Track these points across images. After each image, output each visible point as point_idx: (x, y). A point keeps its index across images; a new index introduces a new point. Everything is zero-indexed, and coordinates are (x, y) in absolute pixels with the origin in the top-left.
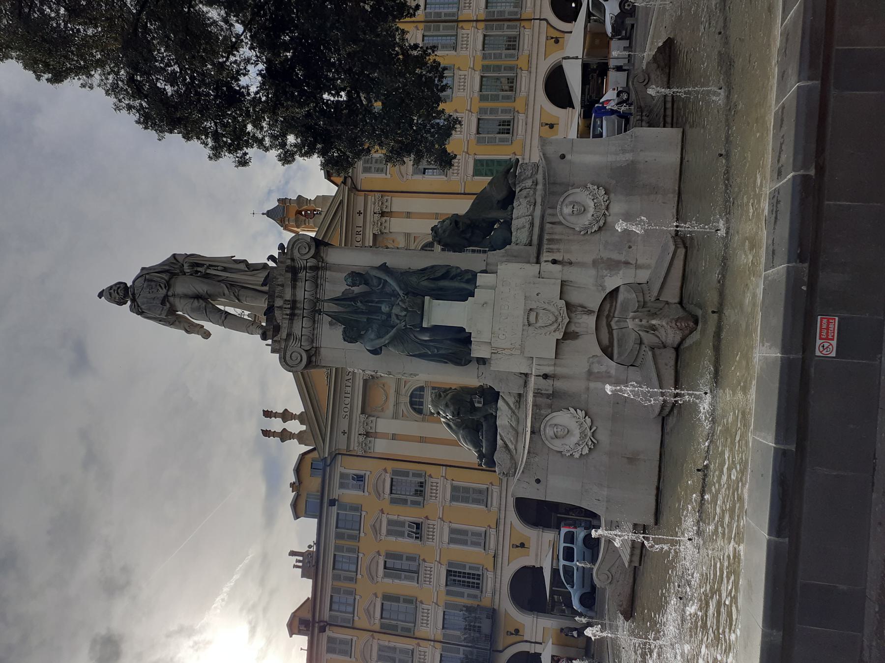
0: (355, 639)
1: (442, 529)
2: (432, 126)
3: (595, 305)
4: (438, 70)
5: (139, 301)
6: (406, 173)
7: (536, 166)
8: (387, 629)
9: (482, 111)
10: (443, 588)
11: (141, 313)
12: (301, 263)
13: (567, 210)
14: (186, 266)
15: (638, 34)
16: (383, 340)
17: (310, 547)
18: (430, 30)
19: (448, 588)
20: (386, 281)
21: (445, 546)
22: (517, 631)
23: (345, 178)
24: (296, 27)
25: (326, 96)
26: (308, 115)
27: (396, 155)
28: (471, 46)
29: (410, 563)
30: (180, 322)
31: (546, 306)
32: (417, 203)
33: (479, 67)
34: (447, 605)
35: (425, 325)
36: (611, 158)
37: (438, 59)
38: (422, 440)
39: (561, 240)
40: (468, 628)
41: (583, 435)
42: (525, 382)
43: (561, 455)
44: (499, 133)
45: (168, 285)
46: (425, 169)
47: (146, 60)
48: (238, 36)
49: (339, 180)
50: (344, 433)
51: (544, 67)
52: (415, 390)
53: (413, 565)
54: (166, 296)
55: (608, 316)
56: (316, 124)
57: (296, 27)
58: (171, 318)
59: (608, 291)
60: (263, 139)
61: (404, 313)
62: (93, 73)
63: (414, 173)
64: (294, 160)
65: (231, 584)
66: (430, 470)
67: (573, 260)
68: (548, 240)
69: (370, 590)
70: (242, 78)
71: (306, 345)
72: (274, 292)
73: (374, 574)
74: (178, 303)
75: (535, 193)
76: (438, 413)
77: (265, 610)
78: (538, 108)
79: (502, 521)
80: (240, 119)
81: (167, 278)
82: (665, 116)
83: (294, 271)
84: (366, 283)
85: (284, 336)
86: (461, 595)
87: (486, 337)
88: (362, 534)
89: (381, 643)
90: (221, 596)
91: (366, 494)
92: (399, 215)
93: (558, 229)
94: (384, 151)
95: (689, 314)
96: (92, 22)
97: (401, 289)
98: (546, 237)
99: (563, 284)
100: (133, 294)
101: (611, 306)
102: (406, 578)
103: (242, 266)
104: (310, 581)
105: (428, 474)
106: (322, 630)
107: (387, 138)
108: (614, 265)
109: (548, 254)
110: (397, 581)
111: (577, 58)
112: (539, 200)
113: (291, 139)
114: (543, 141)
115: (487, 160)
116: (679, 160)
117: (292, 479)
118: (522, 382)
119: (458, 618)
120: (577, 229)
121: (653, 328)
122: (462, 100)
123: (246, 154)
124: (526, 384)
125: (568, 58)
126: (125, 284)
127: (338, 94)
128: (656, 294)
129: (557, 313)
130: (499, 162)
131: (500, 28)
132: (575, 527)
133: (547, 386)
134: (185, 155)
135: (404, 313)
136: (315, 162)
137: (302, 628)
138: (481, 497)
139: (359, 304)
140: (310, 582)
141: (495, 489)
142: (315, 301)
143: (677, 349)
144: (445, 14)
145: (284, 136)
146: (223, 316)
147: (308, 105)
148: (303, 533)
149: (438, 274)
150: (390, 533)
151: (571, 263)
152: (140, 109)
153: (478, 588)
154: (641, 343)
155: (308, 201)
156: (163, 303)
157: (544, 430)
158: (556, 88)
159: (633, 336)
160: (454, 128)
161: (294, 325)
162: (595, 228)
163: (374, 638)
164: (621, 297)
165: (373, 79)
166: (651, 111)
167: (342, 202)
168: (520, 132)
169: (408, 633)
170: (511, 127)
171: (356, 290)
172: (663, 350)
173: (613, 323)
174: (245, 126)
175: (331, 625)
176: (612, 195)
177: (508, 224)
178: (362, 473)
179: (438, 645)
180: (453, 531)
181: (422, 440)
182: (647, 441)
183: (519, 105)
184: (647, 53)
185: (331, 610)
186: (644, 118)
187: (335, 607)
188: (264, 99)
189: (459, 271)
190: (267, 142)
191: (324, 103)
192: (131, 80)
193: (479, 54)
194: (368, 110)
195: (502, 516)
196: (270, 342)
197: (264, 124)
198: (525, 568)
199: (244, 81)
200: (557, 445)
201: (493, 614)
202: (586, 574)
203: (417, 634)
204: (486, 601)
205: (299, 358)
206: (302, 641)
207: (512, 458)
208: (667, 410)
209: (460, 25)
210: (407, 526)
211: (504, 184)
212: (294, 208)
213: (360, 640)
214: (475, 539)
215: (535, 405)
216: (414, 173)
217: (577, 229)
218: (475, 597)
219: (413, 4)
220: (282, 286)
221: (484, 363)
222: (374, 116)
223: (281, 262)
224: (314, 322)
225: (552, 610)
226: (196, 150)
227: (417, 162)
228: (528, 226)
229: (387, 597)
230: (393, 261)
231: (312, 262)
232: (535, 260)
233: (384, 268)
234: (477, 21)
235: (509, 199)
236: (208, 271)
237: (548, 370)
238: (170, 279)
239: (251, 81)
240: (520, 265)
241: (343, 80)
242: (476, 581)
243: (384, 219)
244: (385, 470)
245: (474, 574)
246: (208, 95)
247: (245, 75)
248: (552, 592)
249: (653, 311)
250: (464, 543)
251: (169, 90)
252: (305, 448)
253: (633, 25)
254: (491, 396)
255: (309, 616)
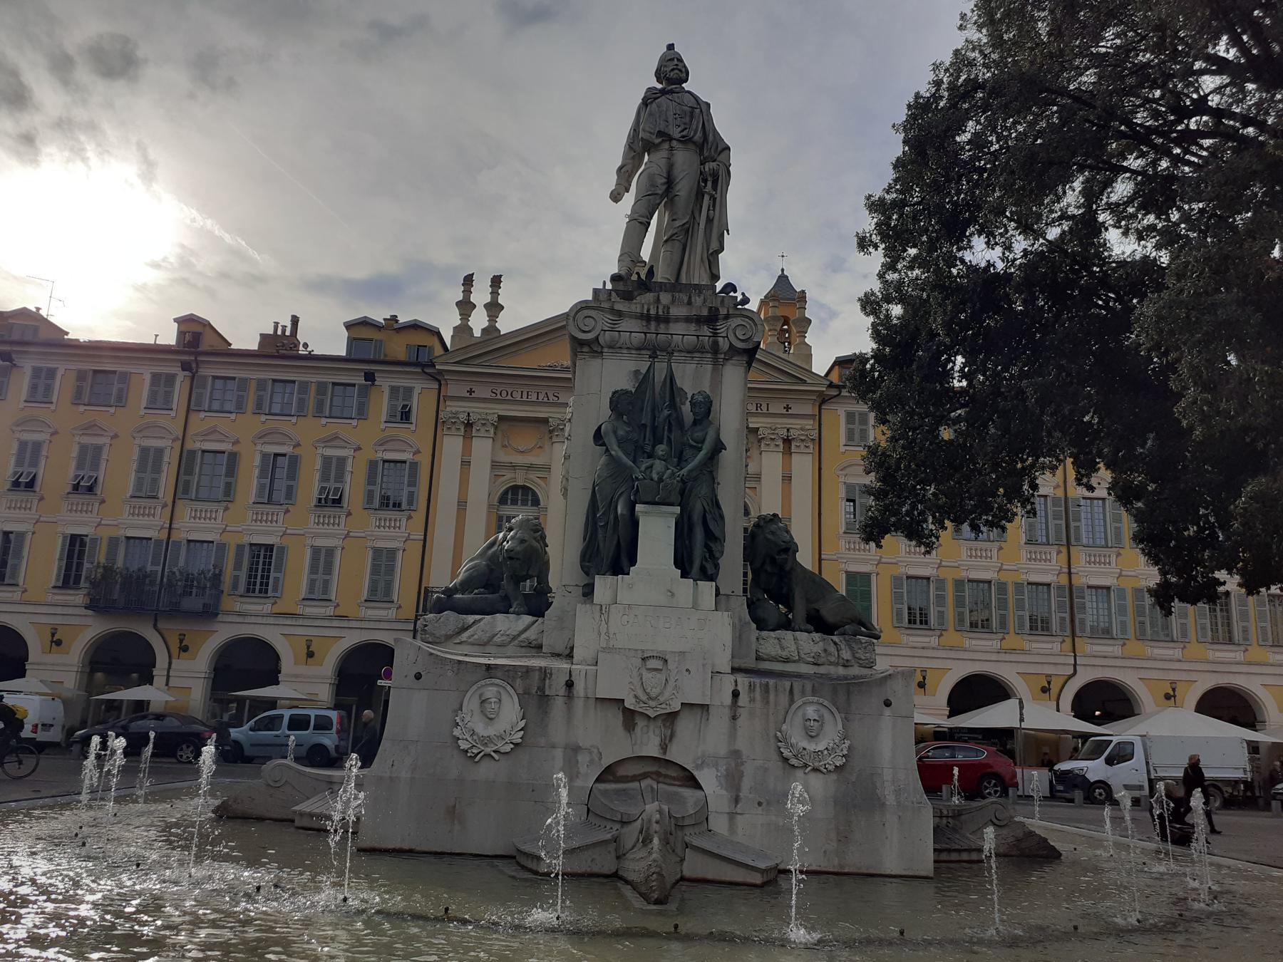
0: (173, 414)
1: (334, 536)
2: (922, 513)
3: (675, 754)
4: (999, 521)
5: (662, 100)
6: (850, 471)
7: (870, 665)
8: (187, 460)
9: (941, 583)
10: (247, 540)
11: (646, 102)
12: (722, 327)
13: (811, 711)
14: (713, 165)
15: (1062, 810)
16: (615, 447)
17: (306, 345)
18: (1054, 505)
19: (247, 549)
20: (700, 450)
21: (309, 542)
22: (184, 649)
23: (838, 387)
24: (1058, 316)
25: (960, 360)
26: (933, 335)
27: (877, 460)
28: (1033, 565)
29: (284, 490)
30: (633, 158)
31: (672, 683)
32: (806, 489)
33: (1004, 577)
34: (222, 547)
35: (639, 507)
36: (887, 774)
37: (1018, 518)
38: (462, 505)
39: (768, 702)
40: (189, 580)
41: (486, 741)
42: (558, 655)
43: (451, 710)
44: (909, 609)
45: (686, 141)
46: (854, 501)
47: (1006, 106)
48: (1041, 234)
49: (834, 378)
50: (471, 392)
51: (1008, 673)
52: (534, 494)
53: (279, 495)
54: (671, 139)
55: (658, 774)
56: (919, 346)
57: (1058, 316)
58: (638, 146)
59: (696, 773)
60: (895, 270)
61: (655, 477)
62: (984, 31)
63: (850, 488)
64: (867, 314)
65: (218, 231)
66: (419, 517)
67: (740, 722)
68: (767, 685)
69: (242, 434)
70: (983, 239)
71: (605, 338)
72: (680, 291)
73: (266, 439)
74: (661, 155)
75: (831, 663)
76: (510, 529)
77: (185, 281)
78: (948, 664)
79: (345, 624)
80: (925, 238)
81: (696, 138)
82: (949, 851)
83: (711, 319)
84: (695, 423)
85: (618, 307)
86: (238, 566)
87: (624, 597)
88: (324, 421)
89: (167, 452)
90: (199, 218)
91: (383, 426)
92: (787, 465)
93: (784, 699)
94: (883, 444)
95: (669, 892)
96: (1055, 32)
97: (690, 471)
98: (772, 682)
99: (704, 708)
100: (672, 92)
101: (674, 778)
102: (261, 487)
103: (714, 246)
104: (255, 347)
105: (413, 514)
106: (185, 366)
107: (903, 447)
108: (733, 781)
109: (747, 684)
110: (135, 466)
111: (1022, 720)
112: (822, 670)
113: (897, 310)
114: (907, 674)
115: (869, 593)
116: (888, 872)
117: (402, 319)
118: (560, 648)
119: (203, 563)
120: (784, 727)
121: (647, 841)
122: (959, 555)
123: (876, 247)
124: (557, 655)
125: (1021, 708)
126: (686, 81)
127: (963, 376)
128: (696, 842)
129: (662, 699)
130: (868, 609)
131: (1060, 607)
132: (338, 732)
133: (556, 687)
134: (876, 160)
135: (655, 477)
136: (866, 345)
137: (188, 337)
138: (380, 592)
139: (666, 412)
140: (254, 346)
141: (392, 613)
142: (668, 350)
143: (616, 876)
144: (1077, 528)
145: (902, 300)
146: (644, 220)
147: (948, 335)
148: (325, 336)
149: (712, 526)
150: (327, 461)
151: (734, 718)
152: (936, 97)
153: (248, 591)
154: (624, 823)
155: (803, 334)
156: (660, 134)
157: (492, 684)
158: (977, 691)
159: (634, 811)
160: (920, 544)
161: (634, 321)
162: (786, 753)
163: (174, 441)
164: (688, 793)
165: (986, 427)
166: (955, 830)
167: (804, 382)
168: (911, 639)
169: (182, 490)
170: (918, 625)
171: (686, 408)
172: (613, 855)
173: (648, 782)
174: (914, 246)
175: (193, 378)
176: (834, 776)
177: (787, 625)
178: (413, 419)
179: (164, 536)
180: (330, 552)
181: (462, 505)
182: (482, 833)
183: (952, 637)
184: (1038, 823)
185: (215, 378)
186: (944, 821)
187: (219, 383)
188: (954, 271)
189: (717, 555)
190: (892, 276)
191: (950, 356)
192: (974, 85)
193: (1023, 578)
194: (942, 420)
195: (353, 624)
196: (609, 286)
197: (917, 272)
198: (277, 658)
199: (979, 242)
200: (471, 703)
201: (210, 613)
202: (279, 749)
203: (179, 503)
204: (228, 603)
205: (587, 329)
206: (169, 337)
207: (449, 637)
208: (529, 864)
209: (1064, 550)
210: (338, 485)
211: (840, 618)
212: (794, 315)
213: (171, 421)
214: (319, 585)
215: (528, 670)
216: (850, 488)
217: (784, 727)
218: (235, 586)
219: (1094, 482)
220: (689, 303)
221: (585, 595)
222: (934, 430)
223: (722, 301)
224: (638, 349)
225: (215, 701)
226: (878, 176)
227: (868, 491)
228: (784, 654)
229: (233, 458)
230: (728, 458)
231: (723, 344)
232: (736, 666)
233: (719, 447)
234: (1070, 573)
235: (820, 624)
236: (706, 198)
237: (579, 688)
238: (695, 143)
239: (980, 253)
240: (729, 644)
241: (983, 383)
242: (258, 587)
243: (780, 443)
244: (417, 452)
245: (267, 584)
246: (959, 192)
247: (988, 243)
248: (241, 701)
249: (672, 839)
250: (314, 569)
251: (963, 138)
252: (447, 337)
253: (1072, 801)
254: (538, 605)
255: (204, 347)
